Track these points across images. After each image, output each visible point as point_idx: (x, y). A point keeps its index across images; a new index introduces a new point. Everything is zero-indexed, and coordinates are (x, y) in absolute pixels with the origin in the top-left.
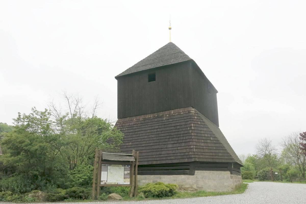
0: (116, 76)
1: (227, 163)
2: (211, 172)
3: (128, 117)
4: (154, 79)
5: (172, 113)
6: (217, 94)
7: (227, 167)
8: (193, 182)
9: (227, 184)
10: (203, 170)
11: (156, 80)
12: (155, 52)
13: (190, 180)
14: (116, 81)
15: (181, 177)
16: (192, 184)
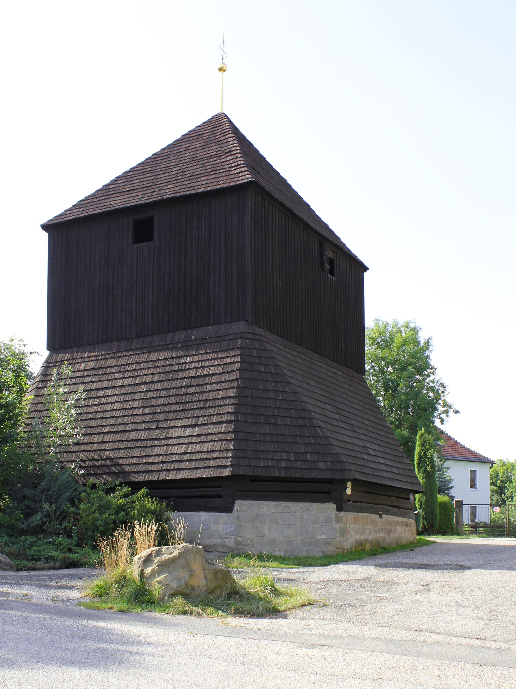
0: (44, 221)
1: (330, 481)
2: (280, 506)
3: (75, 347)
4: (150, 238)
5: (193, 339)
6: (365, 274)
7: (329, 493)
8: (229, 530)
9: (323, 536)
10: (258, 500)
11: (156, 236)
12: (168, 146)
13: (221, 527)
14: (45, 236)
15: (199, 516)
16: (224, 536)
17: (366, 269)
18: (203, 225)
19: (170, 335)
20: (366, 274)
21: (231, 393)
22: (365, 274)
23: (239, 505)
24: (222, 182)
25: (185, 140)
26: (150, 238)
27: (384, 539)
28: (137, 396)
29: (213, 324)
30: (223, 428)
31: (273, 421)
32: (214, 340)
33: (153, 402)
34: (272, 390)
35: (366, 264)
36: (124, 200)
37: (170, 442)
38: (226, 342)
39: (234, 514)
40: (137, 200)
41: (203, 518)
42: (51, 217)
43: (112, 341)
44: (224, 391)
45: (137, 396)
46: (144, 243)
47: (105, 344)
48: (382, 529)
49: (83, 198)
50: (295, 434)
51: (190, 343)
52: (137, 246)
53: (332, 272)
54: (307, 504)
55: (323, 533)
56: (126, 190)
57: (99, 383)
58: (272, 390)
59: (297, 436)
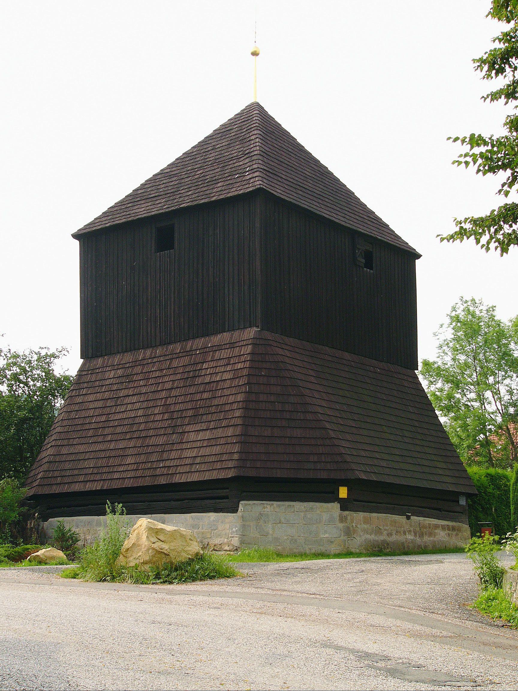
0: (75, 230)
3: (106, 355)
4: (172, 247)
8: (234, 530)
9: (327, 535)
14: (77, 243)
17: (419, 256)
20: (418, 263)
21: (240, 398)
22: (417, 262)
23: (242, 505)
24: (234, 189)
25: (214, 137)
26: (172, 247)
27: (413, 541)
30: (230, 432)
32: (228, 346)
33: (172, 408)
35: (419, 250)
36: (148, 208)
37: (184, 446)
38: (238, 348)
39: (239, 513)
40: (158, 209)
41: (212, 518)
42: (81, 226)
44: (234, 396)
48: (410, 531)
49: (112, 204)
52: (160, 254)
53: (369, 264)
54: (311, 504)
55: (326, 532)
56: (152, 196)
57: (126, 390)
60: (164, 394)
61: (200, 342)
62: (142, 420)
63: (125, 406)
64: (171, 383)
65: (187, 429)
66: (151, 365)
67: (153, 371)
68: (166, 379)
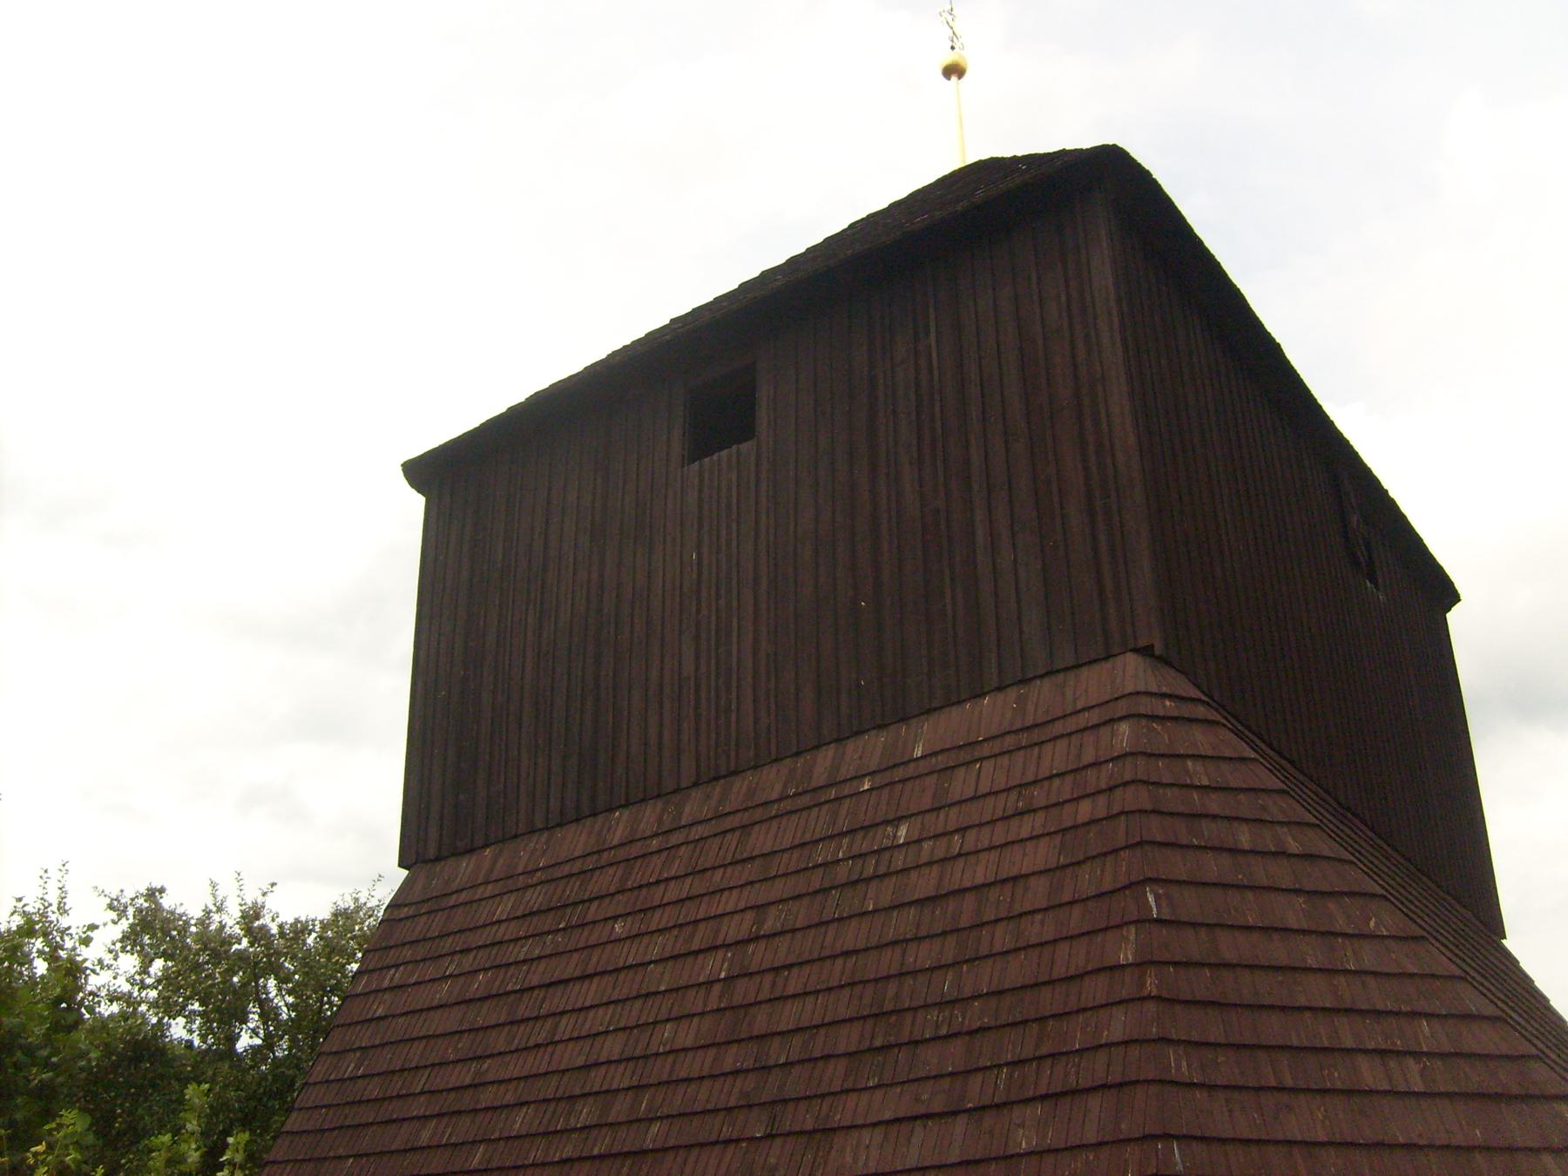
4: (745, 431)
6: (1448, 615)
14: (415, 504)
18: (933, 343)
19: (829, 752)
26: (745, 431)
28: (694, 1001)
29: (1000, 689)
31: (1338, 1076)
33: (761, 1021)
34: (1304, 932)
43: (611, 810)
45: (694, 1001)
46: (724, 453)
47: (589, 822)
50: (1458, 1140)
51: (911, 770)
52: (701, 466)
58: (1304, 932)
59: (1471, 1149)
60: (717, 966)
61: (873, 747)
62: (620, 1077)
63: (549, 1023)
64: (749, 916)
65: (846, 1109)
66: (657, 861)
67: (667, 880)
68: (729, 902)
